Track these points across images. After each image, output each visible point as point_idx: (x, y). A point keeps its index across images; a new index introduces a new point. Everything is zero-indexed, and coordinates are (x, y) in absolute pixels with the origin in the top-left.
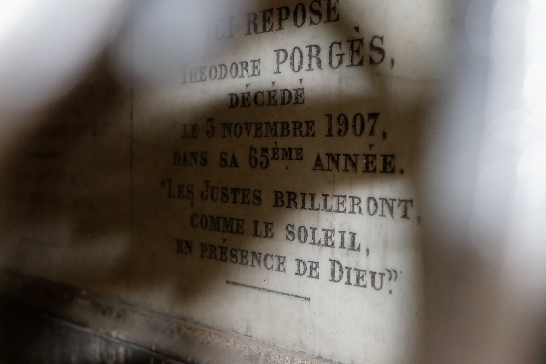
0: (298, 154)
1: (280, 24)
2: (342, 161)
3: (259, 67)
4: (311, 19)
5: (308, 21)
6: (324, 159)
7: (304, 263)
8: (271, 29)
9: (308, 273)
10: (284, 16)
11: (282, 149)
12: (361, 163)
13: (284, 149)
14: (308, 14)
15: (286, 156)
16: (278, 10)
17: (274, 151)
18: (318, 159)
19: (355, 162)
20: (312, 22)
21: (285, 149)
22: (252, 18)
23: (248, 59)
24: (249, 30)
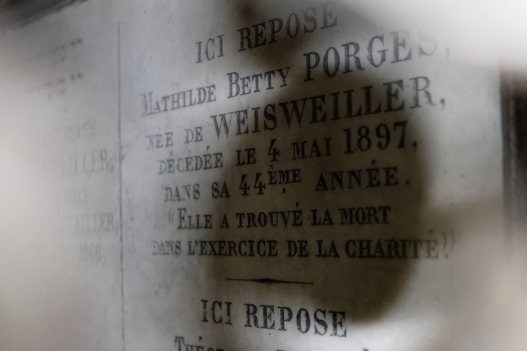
0: (295, 176)
1: (283, 324)
2: (346, 178)
3: (255, 156)
4: (315, 327)
5: (312, 329)
6: (328, 179)
7: (294, 243)
8: (272, 326)
9: (298, 253)
10: (286, 316)
11: (279, 172)
12: (365, 179)
13: (281, 172)
14: (313, 322)
15: (284, 180)
16: (219, 38)
17: (370, 175)
18: (322, 178)
19: (352, 176)
20: (317, 331)
21: (282, 172)
22: (245, 33)
23: (224, 300)
24: (249, 321)
